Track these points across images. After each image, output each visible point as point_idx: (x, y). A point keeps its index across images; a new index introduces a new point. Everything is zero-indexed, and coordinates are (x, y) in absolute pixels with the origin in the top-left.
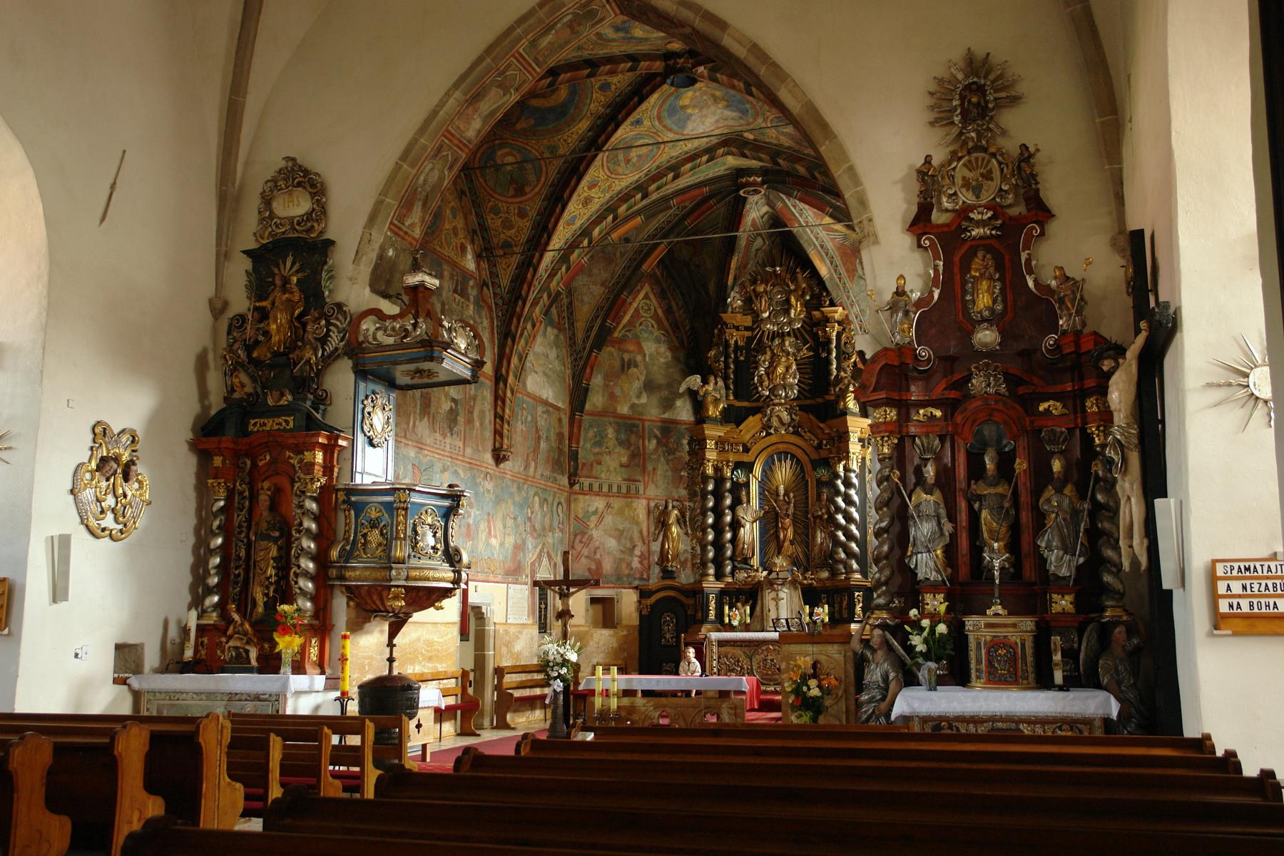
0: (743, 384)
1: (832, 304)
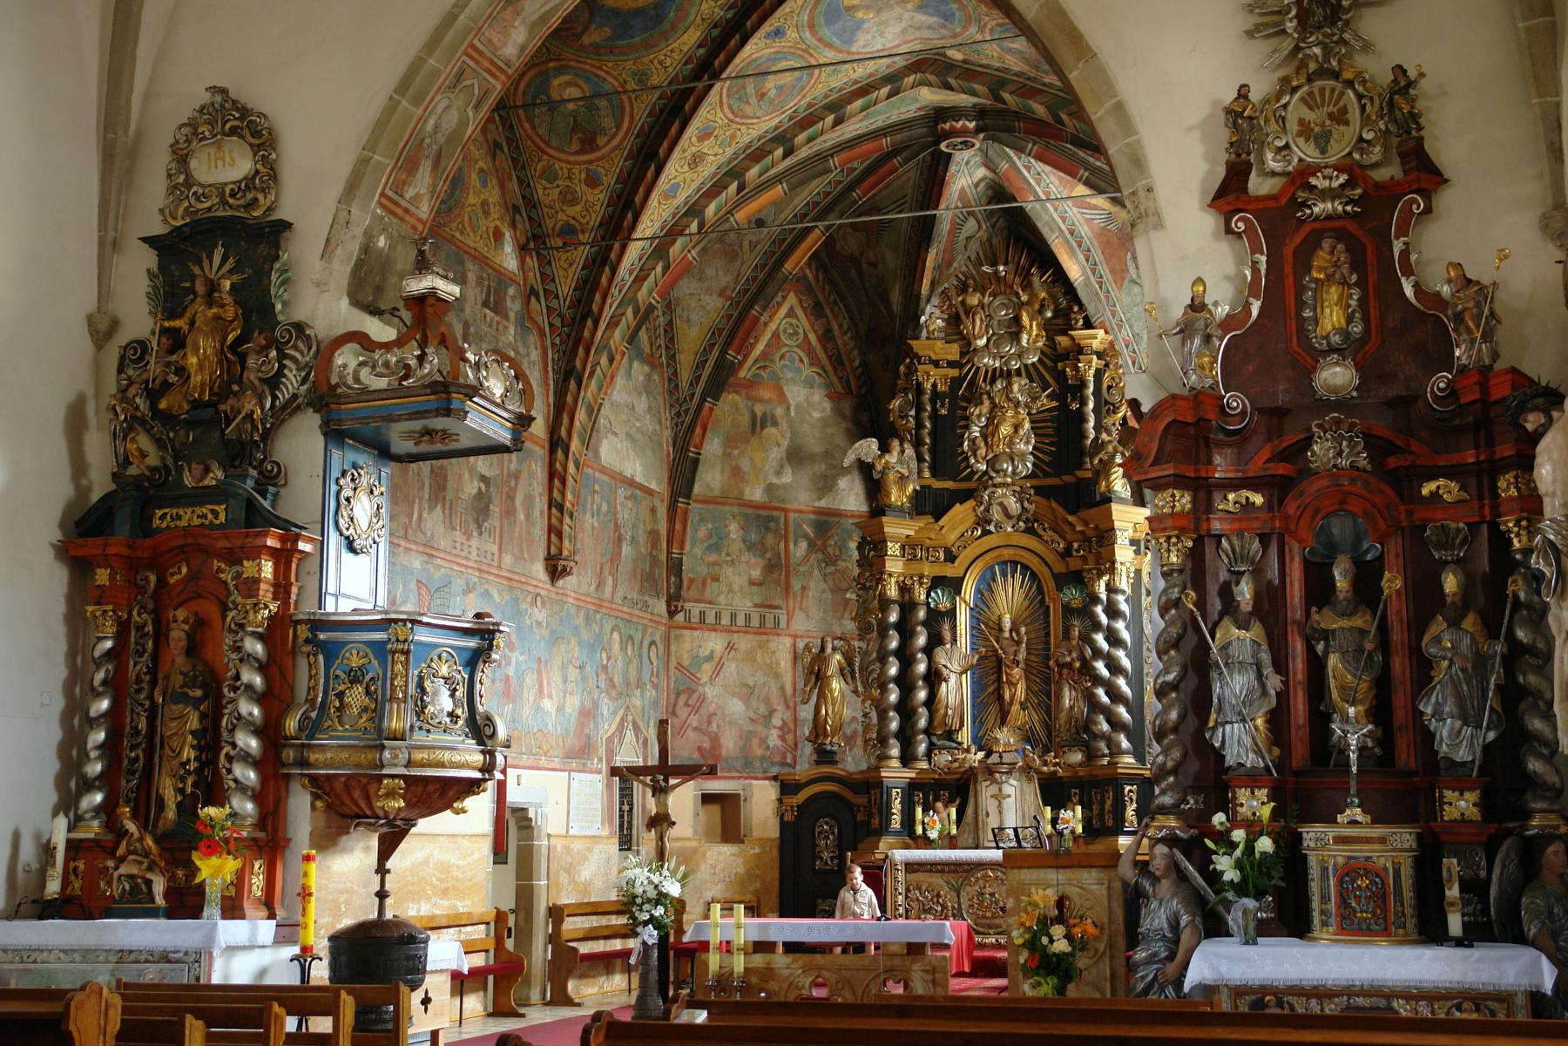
0: (944, 452)
1: (1088, 324)
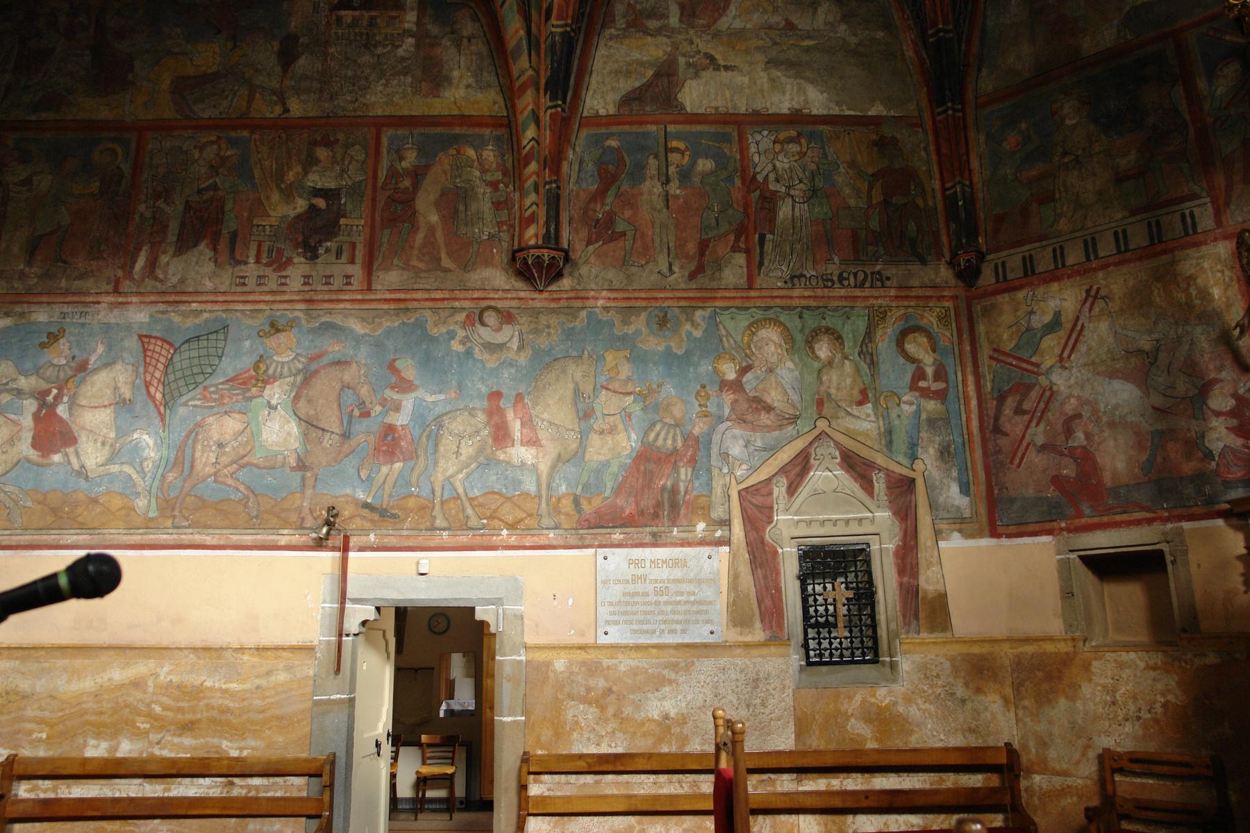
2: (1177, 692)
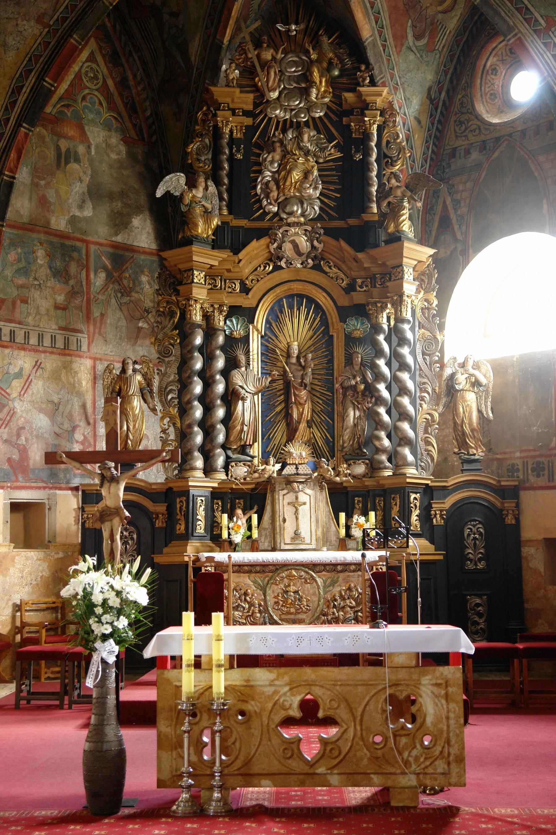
0: (240, 196)
1: (373, 83)
2: (47, 571)
